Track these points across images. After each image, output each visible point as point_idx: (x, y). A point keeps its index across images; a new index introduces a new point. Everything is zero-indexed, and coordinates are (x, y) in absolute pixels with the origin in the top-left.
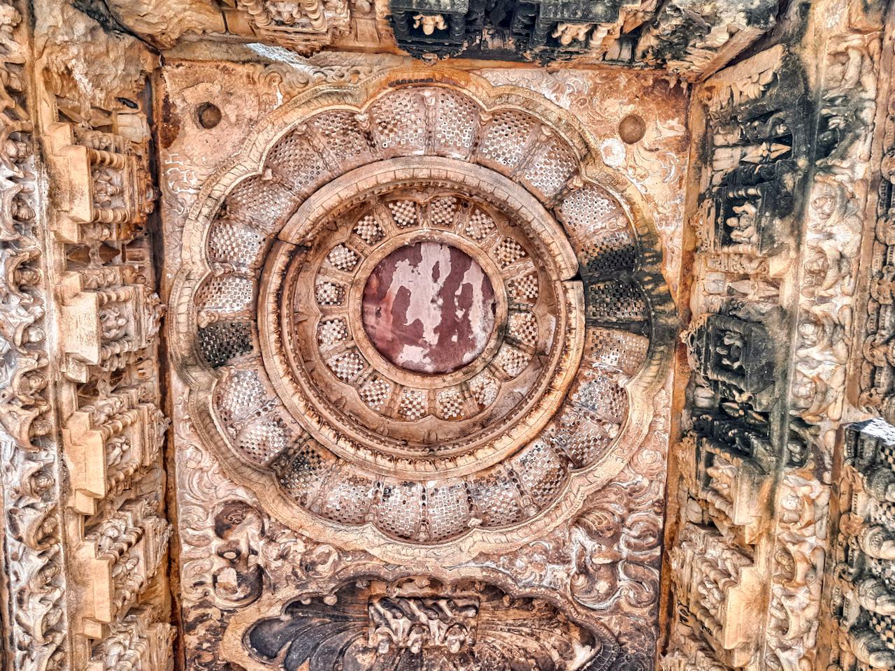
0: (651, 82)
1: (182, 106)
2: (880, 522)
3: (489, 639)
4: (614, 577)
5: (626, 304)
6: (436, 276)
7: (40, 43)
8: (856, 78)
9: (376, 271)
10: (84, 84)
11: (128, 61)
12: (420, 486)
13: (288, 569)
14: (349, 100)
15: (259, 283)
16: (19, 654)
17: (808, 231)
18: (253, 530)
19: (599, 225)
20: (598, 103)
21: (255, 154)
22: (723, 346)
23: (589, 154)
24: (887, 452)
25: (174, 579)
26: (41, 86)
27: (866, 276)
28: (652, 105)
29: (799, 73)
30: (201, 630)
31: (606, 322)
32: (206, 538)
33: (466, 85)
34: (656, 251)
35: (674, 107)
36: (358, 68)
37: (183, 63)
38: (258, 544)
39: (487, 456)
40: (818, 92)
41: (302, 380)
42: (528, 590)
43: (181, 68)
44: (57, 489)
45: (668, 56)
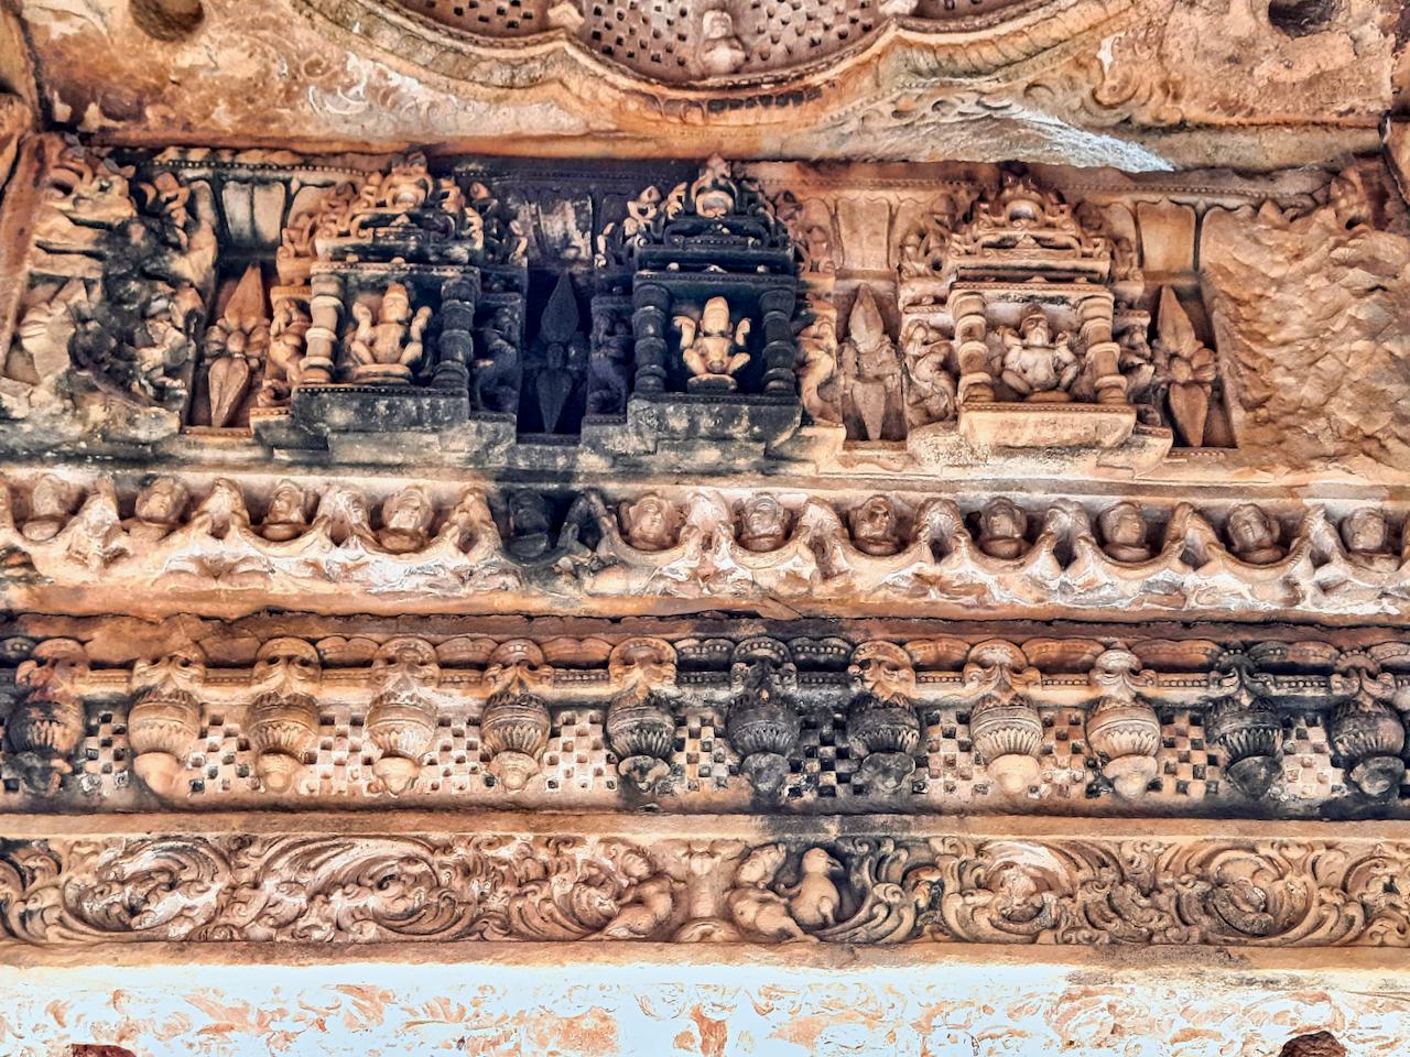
0: (149, 112)
1: (1366, 28)
14: (924, 61)
20: (276, 67)
33: (621, 103)
36: (896, 122)
37: (1334, 118)
43: (1343, 108)
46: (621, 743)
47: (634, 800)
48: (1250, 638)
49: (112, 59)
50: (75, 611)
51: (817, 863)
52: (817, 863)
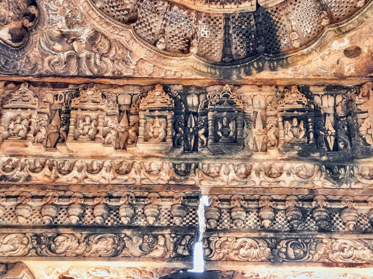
2: (161, 211)
5: (241, 40)
17: (290, 164)
19: (293, 23)
22: (228, 122)
24: (194, 212)
27: (270, 192)
29: (368, 156)
31: (229, 27)
34: (277, 67)
35: (362, 70)
40: (358, 163)
42: (45, 9)
48: (245, 185)
49: (362, 64)
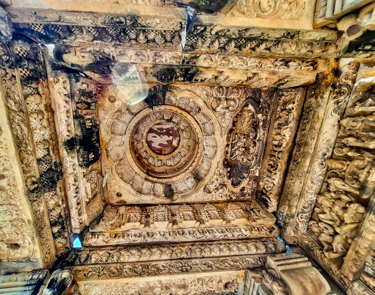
3: (244, 130)
4: (230, 99)
6: (155, 137)
7: (106, 231)
8: (88, 53)
9: (154, 152)
10: (114, 221)
11: (109, 212)
12: (205, 147)
13: (220, 179)
14: (112, 167)
15: (155, 182)
16: (226, 237)
18: (211, 186)
21: (127, 186)
23: (119, 111)
25: (220, 202)
26: (114, 231)
28: (106, 94)
30: (232, 196)
32: (211, 195)
38: (214, 185)
39: (198, 130)
41: (178, 173)
44: (194, 229)
45: (92, 95)
46: (46, 158)
47: (39, 161)
50: (49, 86)
51: (36, 185)
52: (36, 185)
